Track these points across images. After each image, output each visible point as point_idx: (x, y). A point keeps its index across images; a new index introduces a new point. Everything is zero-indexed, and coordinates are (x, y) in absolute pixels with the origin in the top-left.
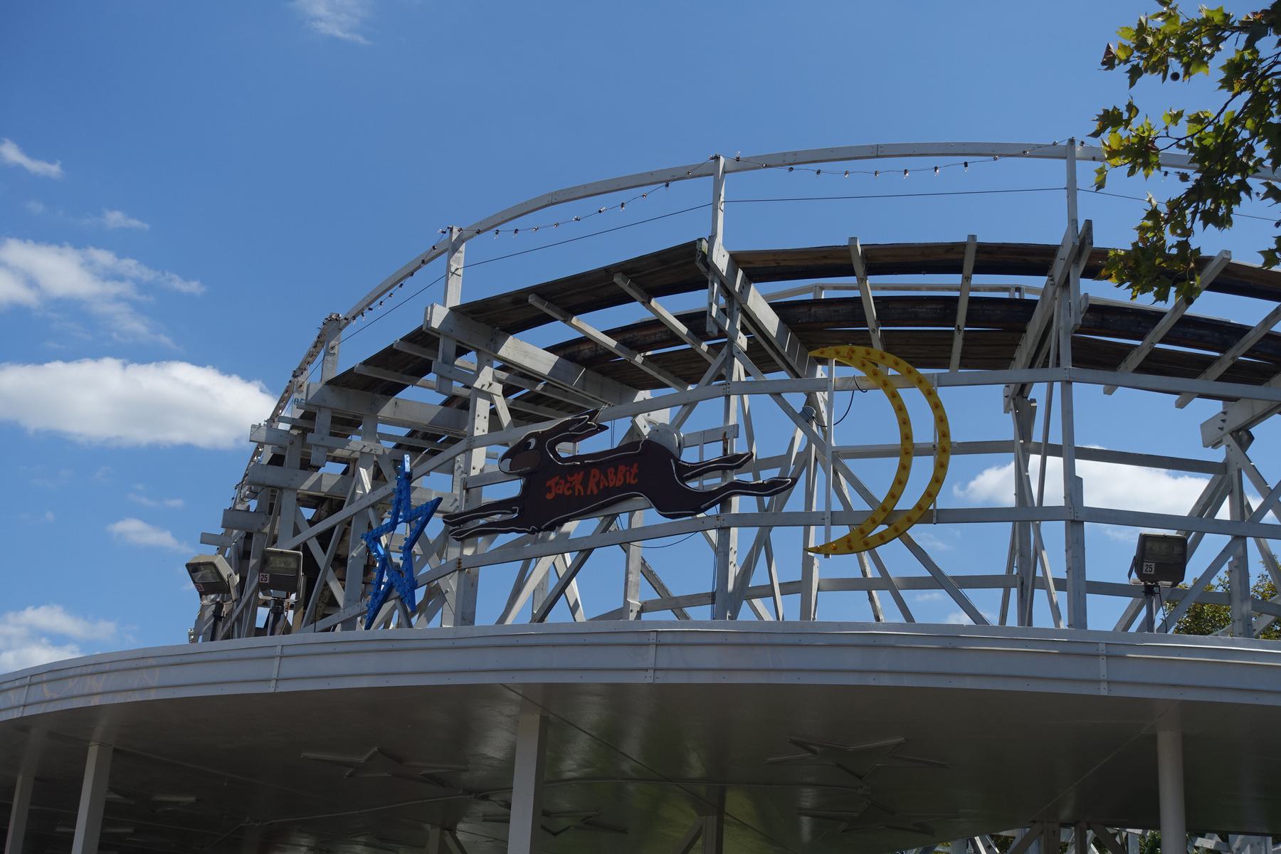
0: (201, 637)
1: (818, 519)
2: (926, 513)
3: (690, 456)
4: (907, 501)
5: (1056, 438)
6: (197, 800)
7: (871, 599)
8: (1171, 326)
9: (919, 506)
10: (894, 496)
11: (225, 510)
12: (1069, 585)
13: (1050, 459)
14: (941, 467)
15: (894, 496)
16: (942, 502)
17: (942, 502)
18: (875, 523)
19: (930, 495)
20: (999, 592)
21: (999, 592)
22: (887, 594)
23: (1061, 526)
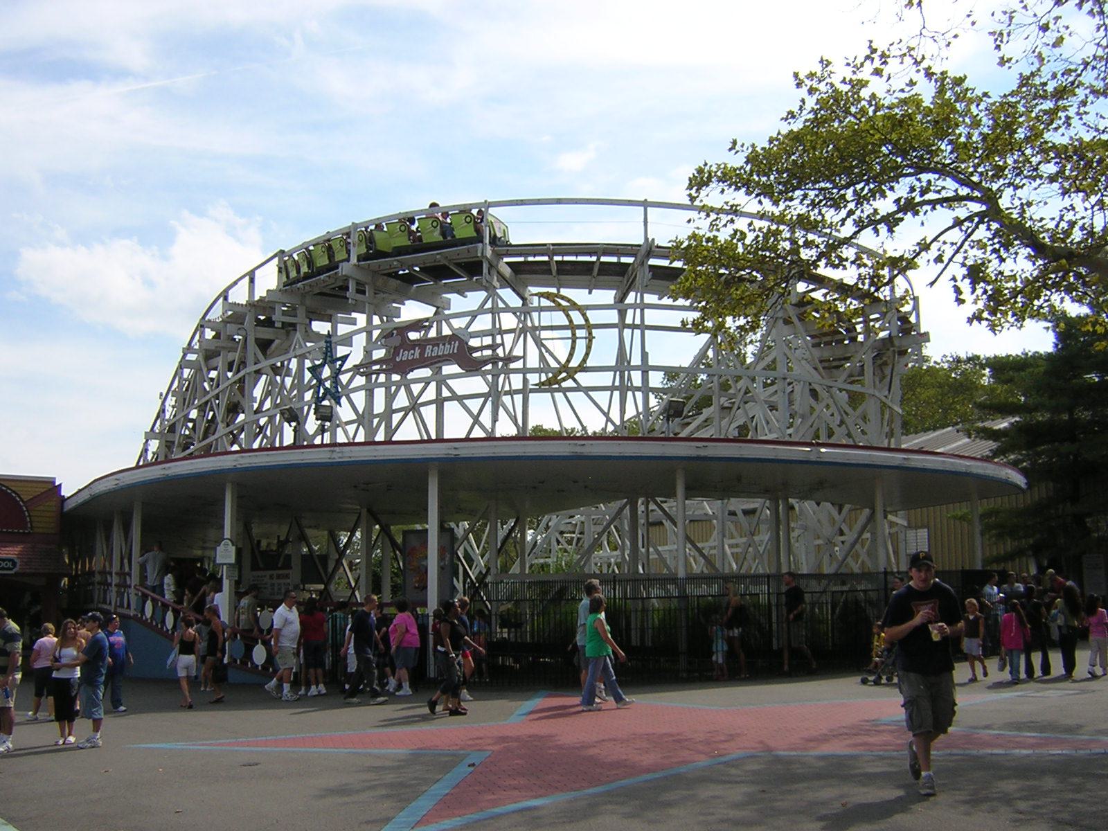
0: (264, 377)
1: (533, 371)
2: (582, 368)
3: (474, 342)
4: (574, 363)
5: (638, 322)
6: (375, 314)
7: (553, 397)
8: (831, 753)
9: (579, 366)
10: (568, 361)
11: (146, 433)
12: (643, 389)
13: (635, 330)
14: (590, 339)
15: (568, 361)
16: (589, 363)
17: (589, 363)
18: (560, 373)
19: (584, 360)
20: (612, 373)
21: (612, 373)
22: (577, 312)
23: (639, 373)
